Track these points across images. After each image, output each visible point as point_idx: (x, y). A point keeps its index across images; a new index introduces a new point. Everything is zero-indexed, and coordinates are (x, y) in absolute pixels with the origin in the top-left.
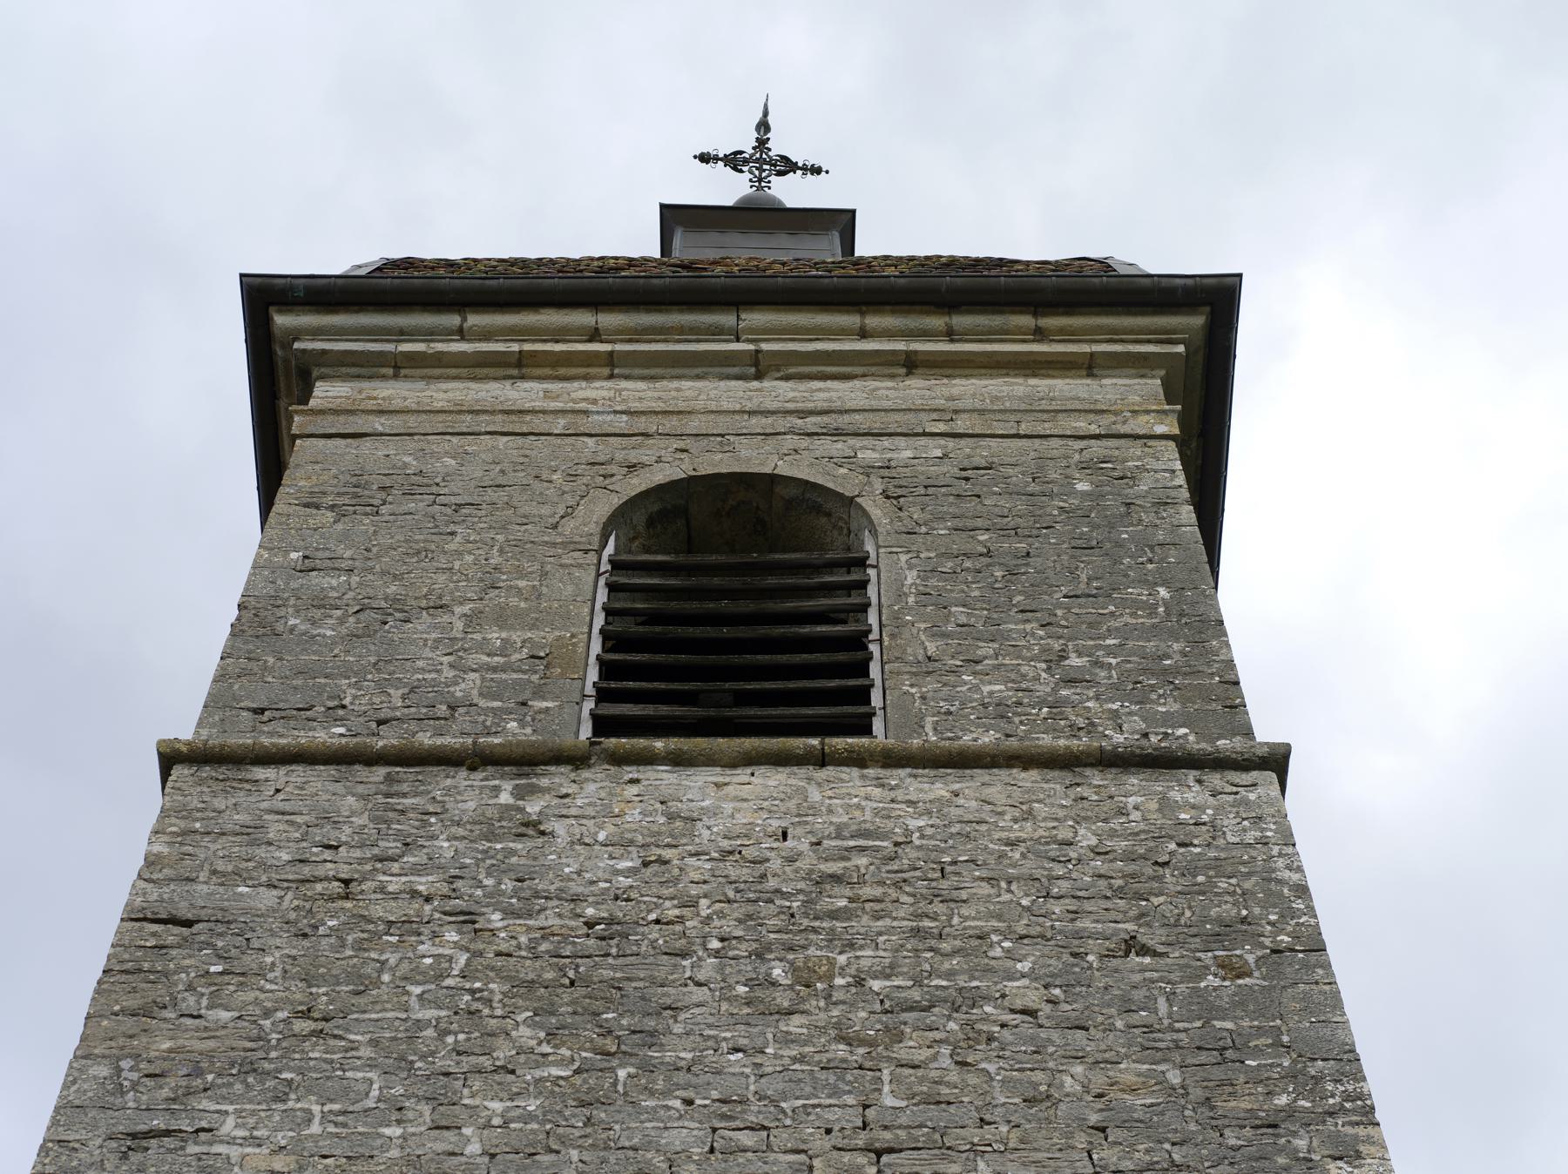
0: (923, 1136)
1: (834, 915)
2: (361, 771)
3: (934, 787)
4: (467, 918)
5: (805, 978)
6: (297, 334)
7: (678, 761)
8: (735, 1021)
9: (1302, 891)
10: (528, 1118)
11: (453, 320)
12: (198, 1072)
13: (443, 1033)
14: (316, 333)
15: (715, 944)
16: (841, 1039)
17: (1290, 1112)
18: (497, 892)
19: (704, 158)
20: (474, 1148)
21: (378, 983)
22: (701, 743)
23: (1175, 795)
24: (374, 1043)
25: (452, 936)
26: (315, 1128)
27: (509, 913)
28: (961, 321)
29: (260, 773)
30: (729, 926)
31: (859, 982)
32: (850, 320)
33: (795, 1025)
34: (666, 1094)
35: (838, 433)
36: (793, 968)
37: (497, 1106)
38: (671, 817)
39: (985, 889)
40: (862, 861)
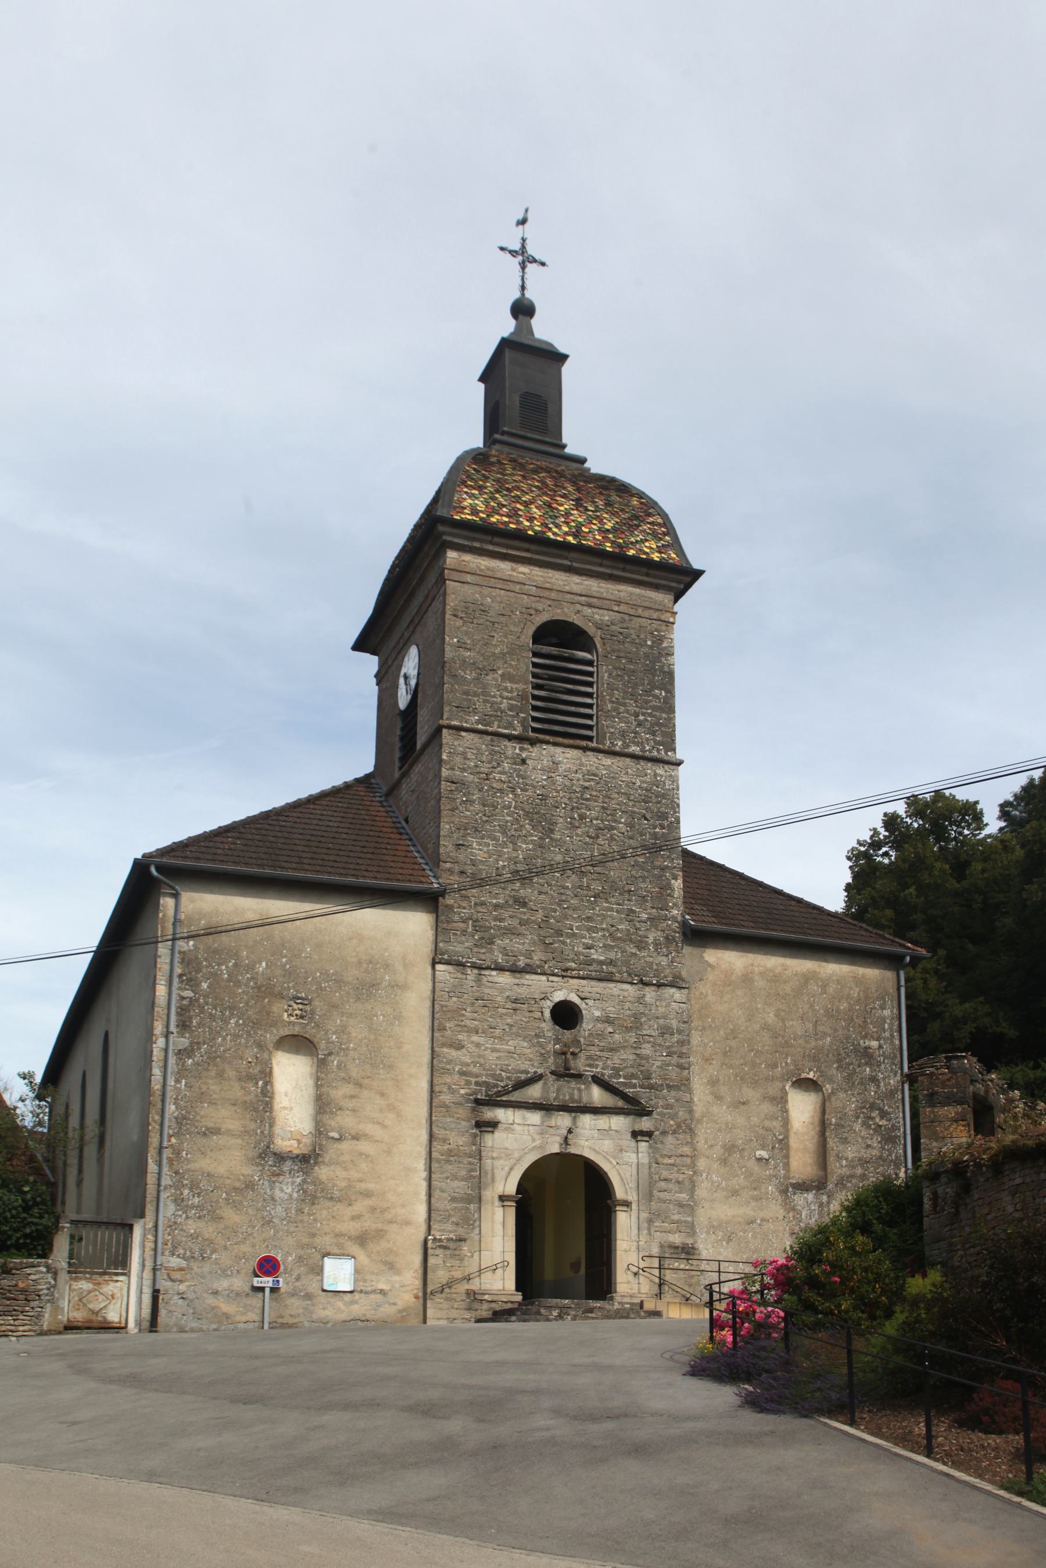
0: (589, 540)
1: (587, 800)
2: (485, 736)
3: (608, 761)
4: (513, 790)
5: (582, 817)
6: (444, 533)
7: (555, 744)
8: (568, 829)
9: (678, 805)
10: (530, 850)
11: (489, 538)
12: (466, 829)
13: (512, 824)
14: (450, 534)
15: (563, 806)
16: (588, 836)
17: (667, 867)
18: (518, 783)
19: (543, 264)
20: (521, 857)
21: (497, 808)
22: (560, 740)
23: (658, 771)
24: (499, 825)
25: (511, 796)
26: (491, 848)
27: (522, 790)
28: (628, 567)
29: (463, 734)
30: (565, 800)
31: (591, 821)
32: (599, 561)
33: (579, 831)
34: (555, 847)
35: (590, 606)
36: (579, 815)
37: (524, 846)
38: (554, 763)
39: (617, 796)
40: (593, 783)
